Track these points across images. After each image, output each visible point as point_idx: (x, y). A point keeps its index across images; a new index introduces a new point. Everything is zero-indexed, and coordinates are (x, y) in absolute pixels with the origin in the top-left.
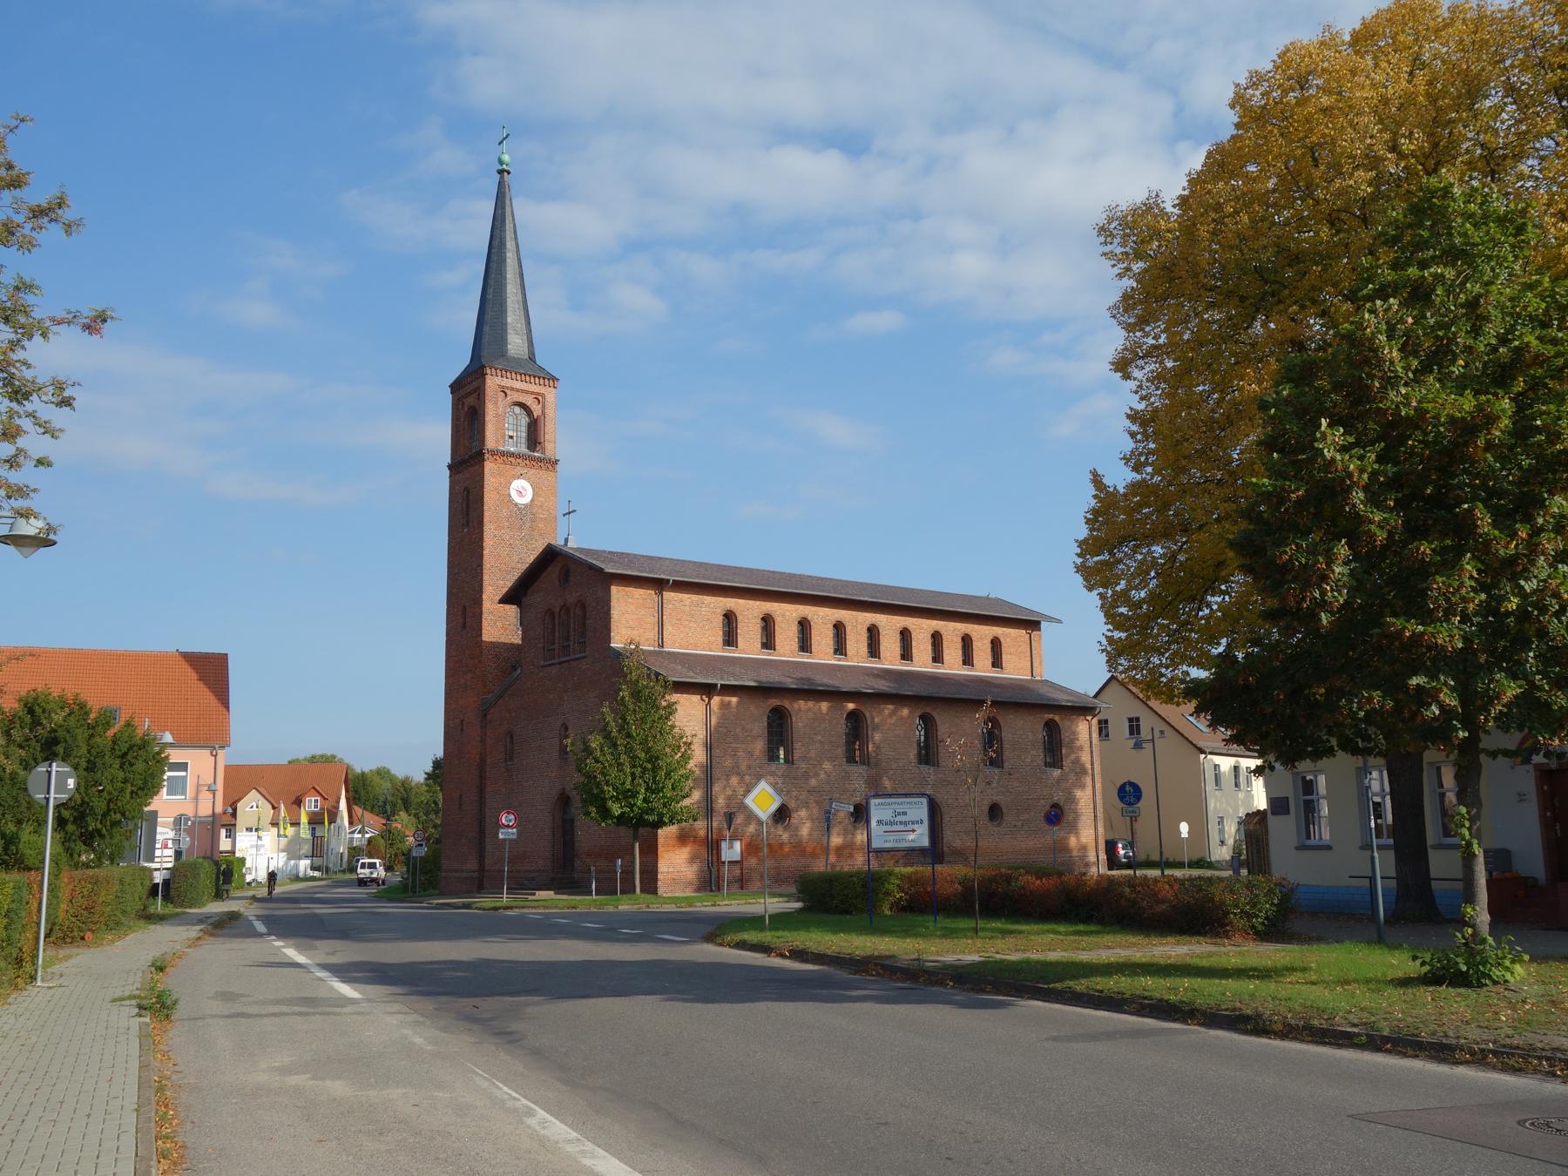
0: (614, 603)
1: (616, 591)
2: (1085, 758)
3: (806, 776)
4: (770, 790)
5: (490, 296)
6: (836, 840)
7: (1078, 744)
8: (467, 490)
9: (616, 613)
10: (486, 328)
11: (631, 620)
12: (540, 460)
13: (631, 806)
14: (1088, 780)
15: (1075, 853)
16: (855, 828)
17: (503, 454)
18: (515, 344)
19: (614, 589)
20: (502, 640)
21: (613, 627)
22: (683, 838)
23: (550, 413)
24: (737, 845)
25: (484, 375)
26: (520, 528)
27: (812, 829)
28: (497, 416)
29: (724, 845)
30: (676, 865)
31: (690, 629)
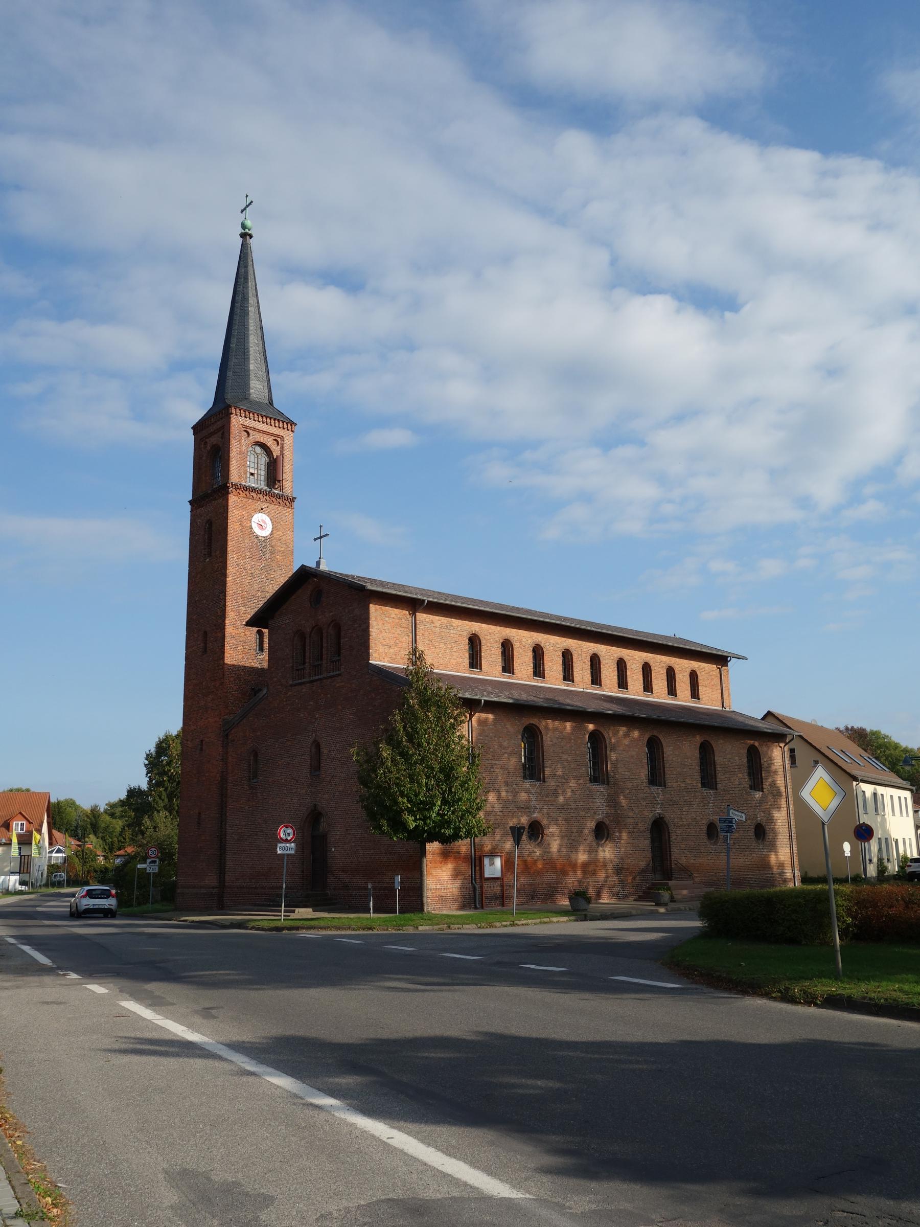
0: (372, 621)
1: (375, 610)
2: (780, 781)
3: (555, 794)
4: (827, 777)
5: (233, 345)
6: (582, 857)
7: (773, 768)
8: (210, 523)
9: (374, 631)
10: (230, 374)
11: (388, 641)
12: (279, 497)
13: (424, 819)
14: (783, 802)
15: (775, 870)
16: (598, 845)
17: (246, 489)
18: (256, 389)
19: (373, 608)
20: (243, 663)
21: (372, 644)
22: (445, 855)
23: (288, 454)
24: (498, 862)
25: (229, 415)
26: (260, 559)
27: (561, 846)
28: (240, 453)
29: (486, 861)
30: (440, 880)
31: (443, 649)
